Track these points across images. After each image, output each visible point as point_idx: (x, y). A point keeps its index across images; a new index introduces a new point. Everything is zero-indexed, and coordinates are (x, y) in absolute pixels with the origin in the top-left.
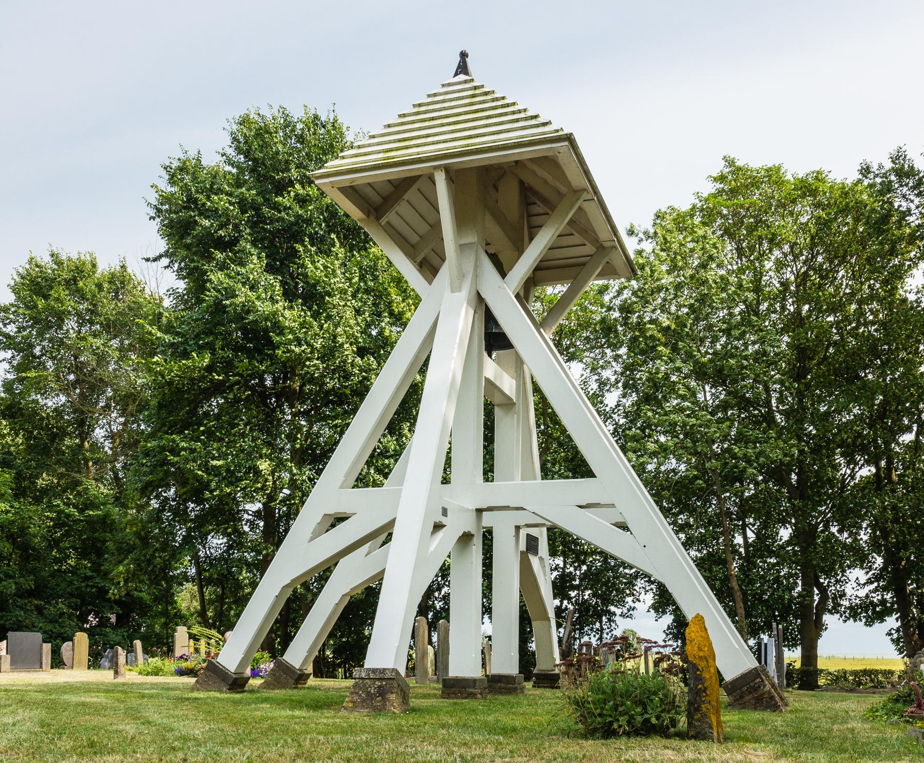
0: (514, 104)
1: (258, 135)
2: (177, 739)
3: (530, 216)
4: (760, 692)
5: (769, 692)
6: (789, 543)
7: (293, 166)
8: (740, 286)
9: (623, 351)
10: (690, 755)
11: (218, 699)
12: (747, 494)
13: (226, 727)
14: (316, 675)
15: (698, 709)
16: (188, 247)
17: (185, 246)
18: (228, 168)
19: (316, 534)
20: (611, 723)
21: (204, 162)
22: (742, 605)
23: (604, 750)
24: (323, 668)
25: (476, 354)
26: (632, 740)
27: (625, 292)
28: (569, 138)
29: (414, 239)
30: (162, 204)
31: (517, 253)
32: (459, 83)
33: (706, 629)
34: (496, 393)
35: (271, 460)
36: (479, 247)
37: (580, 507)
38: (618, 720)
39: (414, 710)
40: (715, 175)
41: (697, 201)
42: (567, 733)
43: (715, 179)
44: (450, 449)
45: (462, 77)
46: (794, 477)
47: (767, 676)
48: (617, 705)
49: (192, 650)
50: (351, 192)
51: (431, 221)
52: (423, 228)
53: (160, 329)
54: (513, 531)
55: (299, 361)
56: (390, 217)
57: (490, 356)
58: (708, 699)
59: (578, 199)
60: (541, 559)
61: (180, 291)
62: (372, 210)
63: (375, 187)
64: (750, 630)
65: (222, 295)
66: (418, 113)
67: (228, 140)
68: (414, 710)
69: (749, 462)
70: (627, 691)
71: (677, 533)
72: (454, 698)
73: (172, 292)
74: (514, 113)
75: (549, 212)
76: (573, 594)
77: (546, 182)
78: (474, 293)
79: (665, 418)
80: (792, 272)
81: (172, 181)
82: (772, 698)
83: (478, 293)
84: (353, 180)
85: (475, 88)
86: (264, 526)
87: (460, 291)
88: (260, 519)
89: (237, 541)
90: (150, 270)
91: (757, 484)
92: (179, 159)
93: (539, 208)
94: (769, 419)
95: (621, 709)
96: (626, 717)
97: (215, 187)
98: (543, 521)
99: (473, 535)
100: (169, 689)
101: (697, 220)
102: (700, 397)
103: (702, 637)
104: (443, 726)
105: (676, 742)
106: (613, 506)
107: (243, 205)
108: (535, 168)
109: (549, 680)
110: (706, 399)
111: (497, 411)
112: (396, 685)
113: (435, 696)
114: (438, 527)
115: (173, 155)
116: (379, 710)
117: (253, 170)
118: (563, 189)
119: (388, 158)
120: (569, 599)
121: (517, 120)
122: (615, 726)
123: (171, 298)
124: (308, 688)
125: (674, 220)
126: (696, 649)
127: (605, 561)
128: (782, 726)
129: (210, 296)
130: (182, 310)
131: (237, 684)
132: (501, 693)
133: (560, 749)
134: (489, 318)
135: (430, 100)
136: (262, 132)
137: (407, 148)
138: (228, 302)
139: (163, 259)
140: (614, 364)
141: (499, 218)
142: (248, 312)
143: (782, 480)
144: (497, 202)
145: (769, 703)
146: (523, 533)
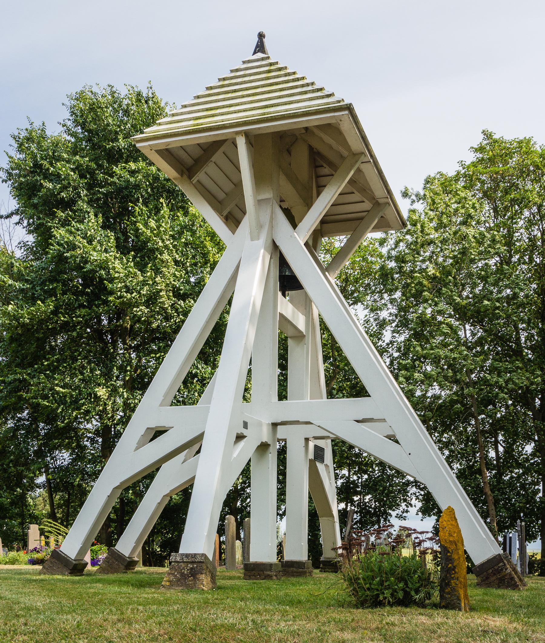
0: (303, 78)
1: (92, 109)
2: (22, 609)
3: (318, 177)
4: (503, 574)
5: (510, 574)
6: (533, 455)
7: (120, 137)
8: (493, 240)
9: (398, 295)
10: (439, 620)
11: (60, 580)
12: (499, 415)
13: (64, 601)
14: (144, 564)
15: (448, 584)
16: (35, 206)
17: (32, 205)
18: (69, 138)
19: (141, 444)
20: (378, 596)
21: (48, 133)
22: (493, 507)
23: (370, 616)
24: (151, 558)
25: (272, 293)
26: (394, 608)
27: (401, 244)
28: (349, 108)
29: (221, 196)
30: (12, 169)
31: (307, 208)
32: (257, 60)
33: (456, 519)
34: (289, 326)
35: (107, 387)
36: (275, 202)
37: (358, 421)
38: (383, 593)
39: (220, 588)
40: (477, 147)
41: (461, 168)
42: (341, 605)
43: (476, 150)
44: (250, 371)
45: (260, 55)
46: (538, 402)
47: (509, 562)
48: (383, 581)
49: (43, 543)
50: (167, 154)
51: (235, 181)
52: (228, 187)
53: (11, 277)
54: (303, 442)
55: (131, 305)
56: (200, 176)
57: (284, 295)
58: (456, 575)
59: (357, 162)
60: (327, 466)
61: (30, 243)
62: (185, 170)
63: (187, 150)
64: (499, 528)
65: (64, 248)
66: (223, 86)
67: (67, 115)
68: (220, 588)
69: (500, 388)
70: (391, 570)
71: (441, 449)
72: (253, 579)
73: (23, 245)
74: (303, 86)
75: (334, 173)
76: (356, 498)
77: (331, 147)
78: (270, 241)
79: (432, 352)
80: (539, 229)
81: (21, 148)
82: (512, 579)
83: (274, 242)
84: (168, 144)
85: (271, 64)
86: (102, 442)
87: (258, 239)
88: (99, 436)
89: (79, 453)
90: (4, 226)
91: (507, 407)
92: (27, 130)
93: (326, 170)
94: (518, 353)
95: (386, 584)
96: (391, 591)
97: (56, 154)
98: (327, 434)
99: (269, 445)
100: (21, 574)
101: (461, 184)
102: (461, 334)
103: (452, 525)
104: (242, 599)
105: (429, 611)
106: (384, 420)
107: (78, 169)
108: (322, 135)
109: (332, 566)
110: (466, 336)
111: (290, 342)
112: (205, 567)
113: (239, 578)
114: (240, 437)
115: (21, 127)
116: (190, 588)
117: (89, 140)
118: (345, 153)
119: (198, 125)
120: (352, 502)
121: (306, 93)
122: (381, 598)
123: (22, 250)
124: (136, 573)
125: (442, 184)
126: (447, 535)
127: (383, 471)
128: (518, 600)
129: (54, 249)
130: (32, 260)
131: (77, 568)
132: (293, 576)
133: (335, 615)
134: (283, 263)
135: (233, 74)
136: (94, 108)
137: (213, 116)
138: (68, 255)
139: (14, 216)
140: (390, 306)
141: (292, 178)
142: (86, 262)
143: (529, 405)
144: (290, 165)
145: (510, 583)
146: (311, 444)
